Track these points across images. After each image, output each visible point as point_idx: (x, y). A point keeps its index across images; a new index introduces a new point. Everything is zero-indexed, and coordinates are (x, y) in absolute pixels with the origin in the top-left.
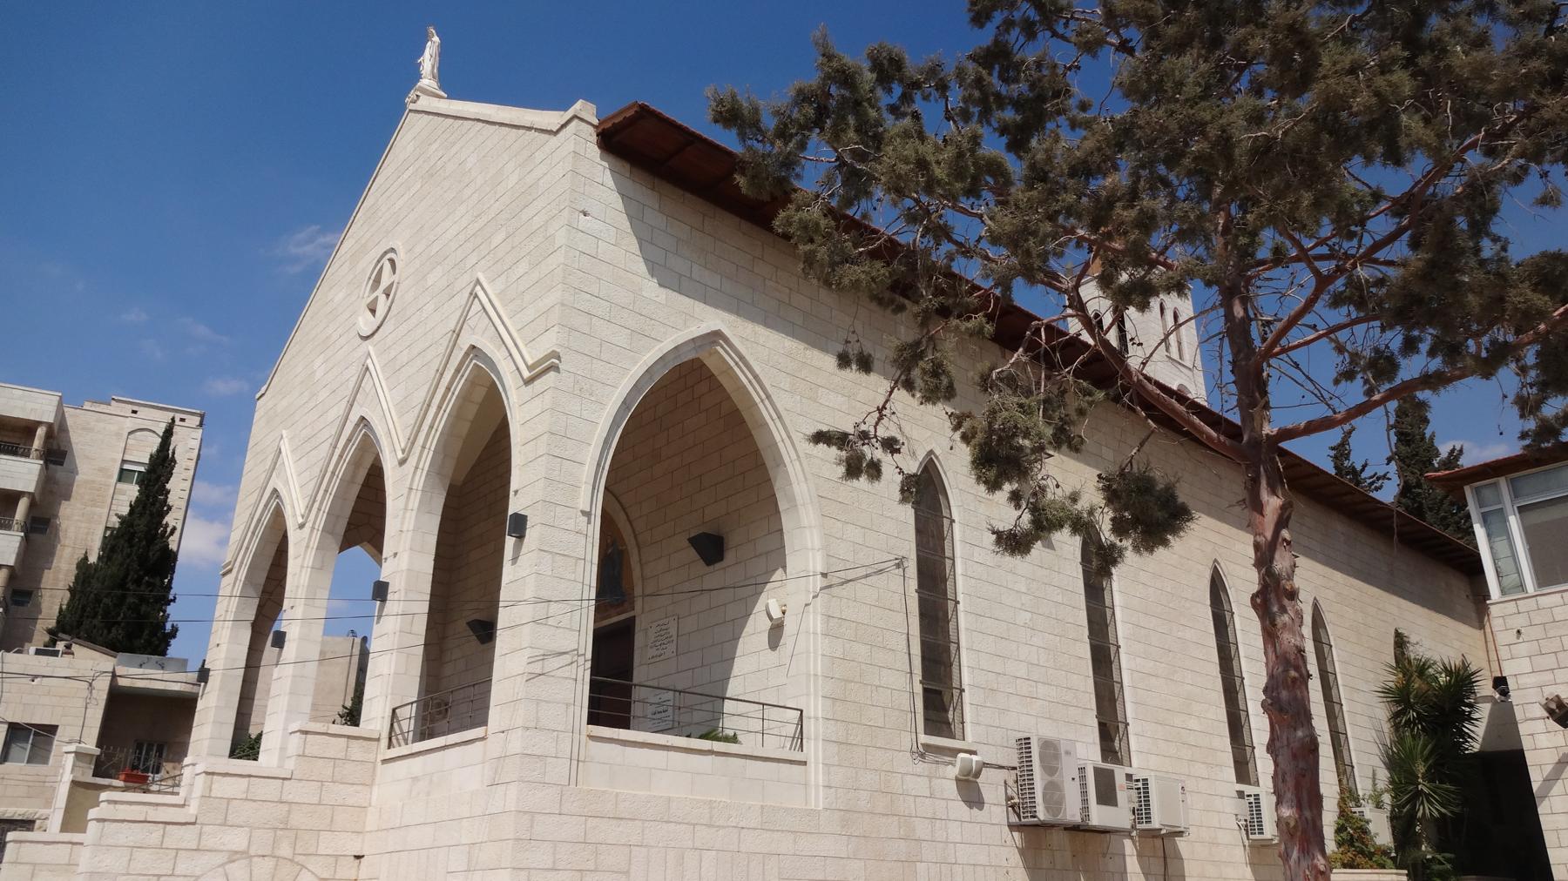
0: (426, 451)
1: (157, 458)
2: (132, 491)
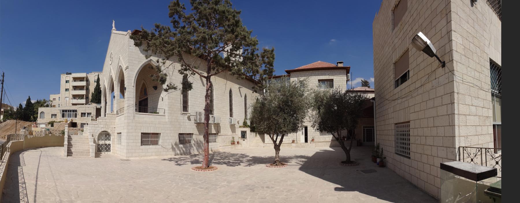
2: (96, 84)
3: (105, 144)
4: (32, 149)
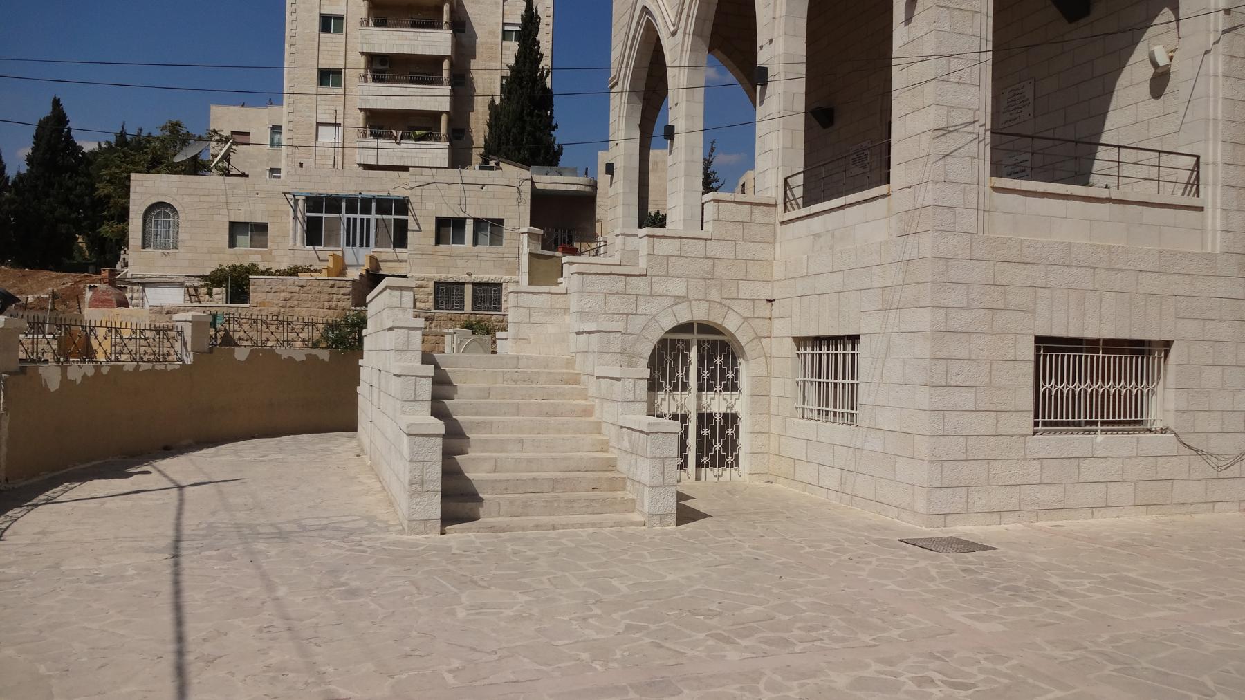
0: (690, 18)
1: (526, 17)
2: (513, 46)
3: (700, 417)
4: (84, 477)
